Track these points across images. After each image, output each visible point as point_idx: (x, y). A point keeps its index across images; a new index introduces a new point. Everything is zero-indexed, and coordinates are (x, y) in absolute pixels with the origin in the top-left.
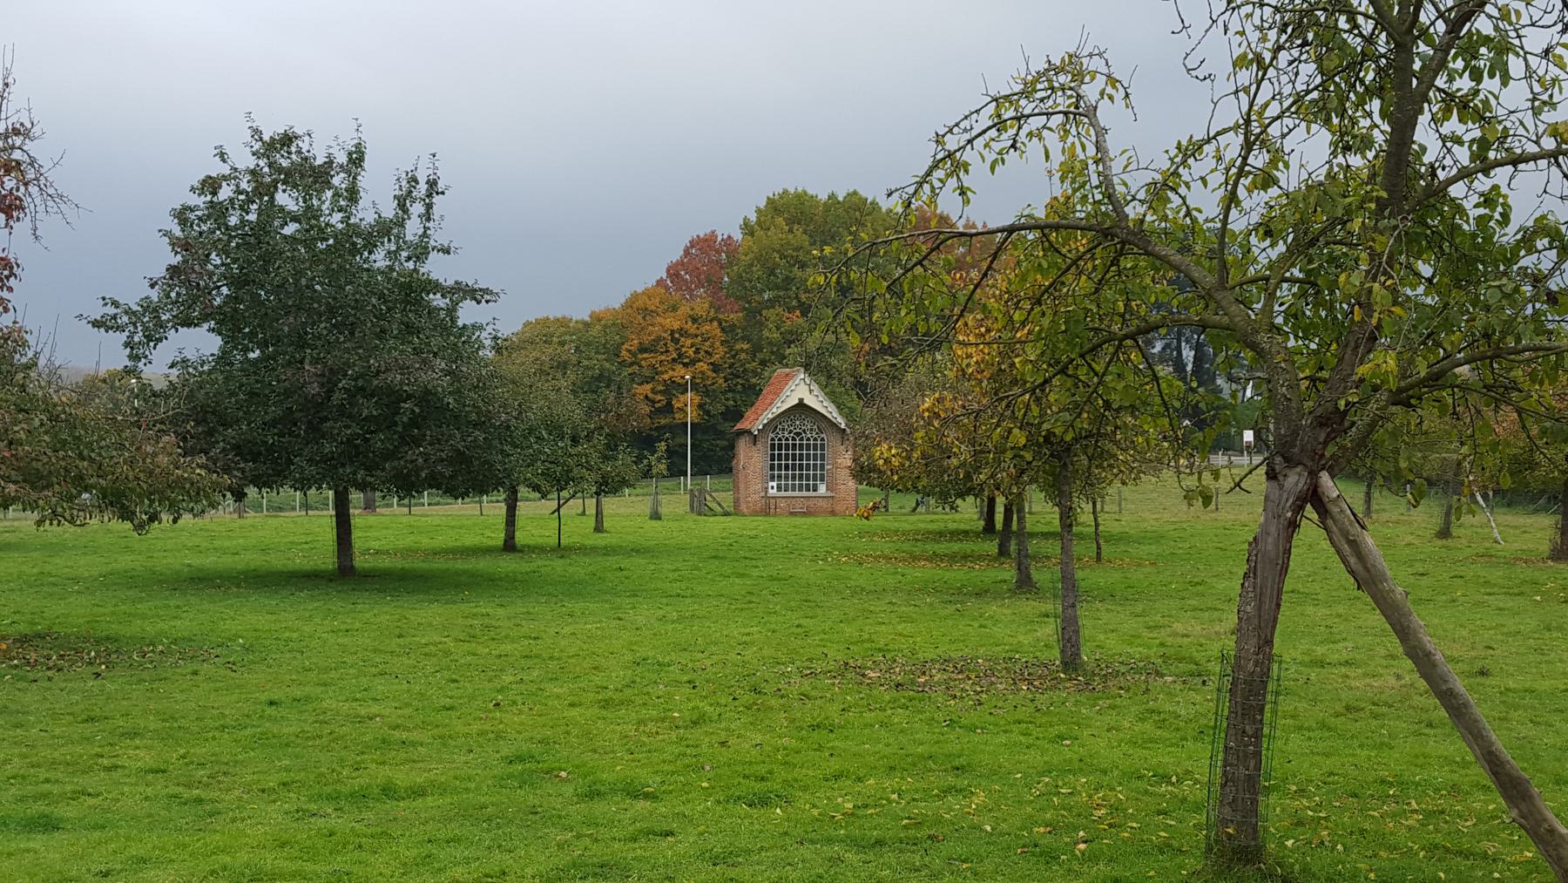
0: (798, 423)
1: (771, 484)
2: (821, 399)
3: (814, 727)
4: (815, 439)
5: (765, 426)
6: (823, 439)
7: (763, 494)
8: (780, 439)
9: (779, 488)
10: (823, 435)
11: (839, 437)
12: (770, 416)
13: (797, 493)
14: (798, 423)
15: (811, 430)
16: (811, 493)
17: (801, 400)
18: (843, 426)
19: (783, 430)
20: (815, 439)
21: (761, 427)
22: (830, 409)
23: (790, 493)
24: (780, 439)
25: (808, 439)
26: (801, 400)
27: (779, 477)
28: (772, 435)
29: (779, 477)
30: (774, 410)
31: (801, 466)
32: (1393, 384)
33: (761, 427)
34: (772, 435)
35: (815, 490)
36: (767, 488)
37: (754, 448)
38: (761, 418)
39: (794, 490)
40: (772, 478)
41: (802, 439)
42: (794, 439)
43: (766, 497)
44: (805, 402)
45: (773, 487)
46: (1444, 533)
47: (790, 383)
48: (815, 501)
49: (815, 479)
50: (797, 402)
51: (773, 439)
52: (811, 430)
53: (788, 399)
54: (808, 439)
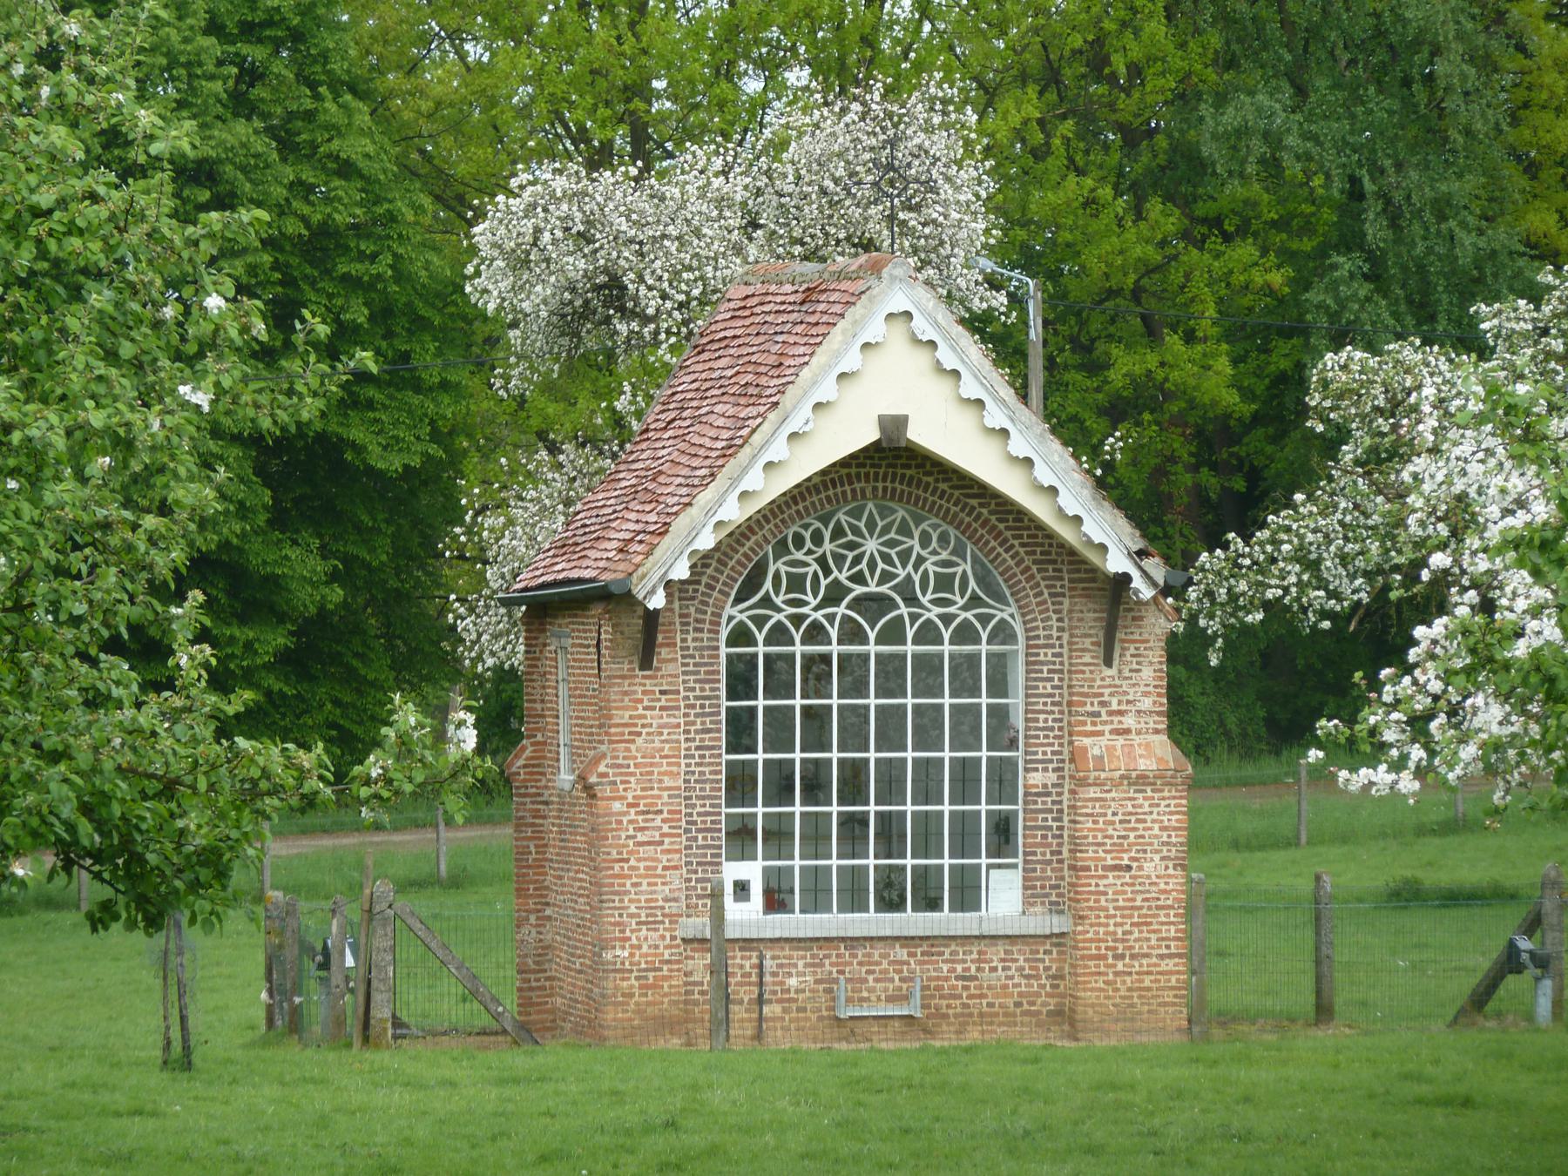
0: (871, 546)
1: (733, 871)
2: (996, 417)
3: (494, 1139)
4: (965, 634)
5: (701, 562)
6: (1002, 633)
7: (699, 925)
8: (779, 635)
9: (775, 901)
10: (1001, 614)
11: (1090, 620)
12: (734, 513)
13: (871, 921)
14: (871, 546)
15: (944, 583)
16: (945, 920)
17: (893, 426)
18: (1117, 563)
19: (796, 583)
20: (965, 634)
21: (681, 571)
22: (1045, 476)
23: (833, 922)
24: (779, 635)
25: (928, 634)
26: (893, 426)
27: (778, 835)
28: (737, 614)
29: (778, 835)
30: (754, 480)
31: (854, 777)
32: (59, 864)
33: (681, 571)
34: (737, 614)
35: (967, 894)
36: (716, 895)
37: (642, 684)
38: (680, 525)
39: (930, 903)
40: (741, 837)
41: (893, 633)
42: (852, 633)
43: (718, 945)
44: (920, 434)
45: (742, 889)
46: (1318, 878)
47: (837, 335)
48: (968, 961)
49: (964, 842)
50: (871, 435)
51: (741, 636)
52: (944, 583)
53: (827, 420)
54: (928, 634)
